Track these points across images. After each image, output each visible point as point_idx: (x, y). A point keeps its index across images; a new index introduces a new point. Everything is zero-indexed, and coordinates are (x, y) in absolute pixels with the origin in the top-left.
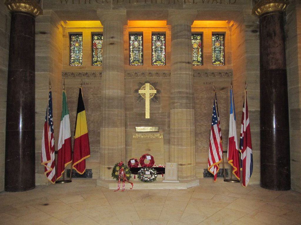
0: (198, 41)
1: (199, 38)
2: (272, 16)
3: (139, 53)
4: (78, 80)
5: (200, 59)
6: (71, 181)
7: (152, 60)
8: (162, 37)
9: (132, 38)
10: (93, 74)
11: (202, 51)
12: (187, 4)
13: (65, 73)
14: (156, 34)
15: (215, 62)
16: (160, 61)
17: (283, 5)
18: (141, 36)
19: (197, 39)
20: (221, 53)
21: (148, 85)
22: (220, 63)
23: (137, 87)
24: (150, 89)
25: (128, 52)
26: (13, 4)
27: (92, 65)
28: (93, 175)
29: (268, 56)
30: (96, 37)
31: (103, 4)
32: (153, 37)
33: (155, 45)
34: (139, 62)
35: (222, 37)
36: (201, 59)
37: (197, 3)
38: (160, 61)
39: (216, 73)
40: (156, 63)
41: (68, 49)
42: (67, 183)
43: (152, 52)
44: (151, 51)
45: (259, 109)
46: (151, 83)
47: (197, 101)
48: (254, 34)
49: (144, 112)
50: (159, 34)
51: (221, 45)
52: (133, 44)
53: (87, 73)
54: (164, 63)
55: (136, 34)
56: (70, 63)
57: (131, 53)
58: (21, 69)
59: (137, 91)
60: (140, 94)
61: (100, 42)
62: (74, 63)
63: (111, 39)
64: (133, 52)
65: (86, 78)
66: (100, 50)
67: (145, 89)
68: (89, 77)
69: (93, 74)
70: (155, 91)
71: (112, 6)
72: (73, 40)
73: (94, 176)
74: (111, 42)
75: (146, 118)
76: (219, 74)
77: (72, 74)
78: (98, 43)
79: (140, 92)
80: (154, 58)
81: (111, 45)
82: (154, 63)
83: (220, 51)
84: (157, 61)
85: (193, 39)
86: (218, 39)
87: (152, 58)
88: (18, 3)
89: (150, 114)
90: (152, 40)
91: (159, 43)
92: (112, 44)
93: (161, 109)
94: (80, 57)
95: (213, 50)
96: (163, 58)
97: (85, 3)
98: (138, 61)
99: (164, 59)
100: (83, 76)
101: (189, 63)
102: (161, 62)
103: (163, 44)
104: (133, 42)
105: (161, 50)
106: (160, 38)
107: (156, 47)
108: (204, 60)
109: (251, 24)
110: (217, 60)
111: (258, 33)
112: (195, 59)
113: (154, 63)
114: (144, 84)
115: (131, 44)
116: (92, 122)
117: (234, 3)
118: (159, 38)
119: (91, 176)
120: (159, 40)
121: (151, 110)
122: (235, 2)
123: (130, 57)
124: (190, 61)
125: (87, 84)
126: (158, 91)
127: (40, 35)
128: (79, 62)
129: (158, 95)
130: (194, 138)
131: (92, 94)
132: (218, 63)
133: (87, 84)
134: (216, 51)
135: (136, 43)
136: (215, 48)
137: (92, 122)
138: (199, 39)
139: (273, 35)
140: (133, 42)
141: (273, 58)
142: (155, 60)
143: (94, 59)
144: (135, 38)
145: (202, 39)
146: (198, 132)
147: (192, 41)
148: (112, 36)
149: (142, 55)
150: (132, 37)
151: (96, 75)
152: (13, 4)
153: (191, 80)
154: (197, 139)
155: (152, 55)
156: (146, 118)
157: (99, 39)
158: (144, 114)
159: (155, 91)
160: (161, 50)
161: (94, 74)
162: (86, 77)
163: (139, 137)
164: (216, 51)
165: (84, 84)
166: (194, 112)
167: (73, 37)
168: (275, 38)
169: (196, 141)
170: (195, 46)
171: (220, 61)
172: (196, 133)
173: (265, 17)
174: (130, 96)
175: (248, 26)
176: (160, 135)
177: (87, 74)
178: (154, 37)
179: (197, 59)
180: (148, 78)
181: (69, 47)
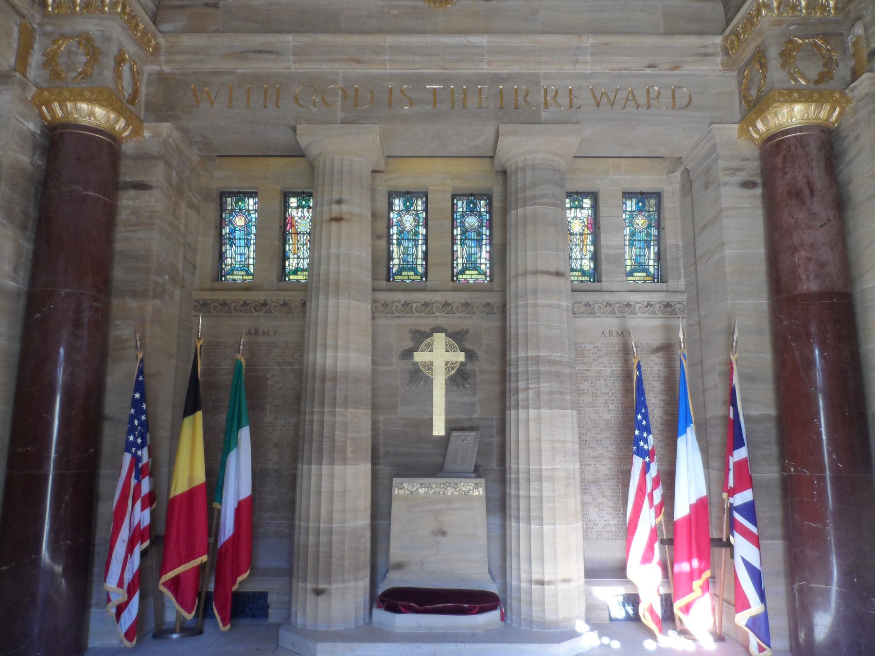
0: (586, 213)
1: (587, 203)
2: (800, 141)
3: (417, 247)
4: (244, 322)
5: (588, 265)
6: (200, 632)
7: (453, 268)
8: (482, 202)
9: (398, 204)
10: (282, 305)
11: (596, 242)
12: (551, 108)
13: (201, 302)
14: (464, 195)
15: (631, 274)
16: (413, 271)
17: (833, 110)
18: (422, 198)
19: (582, 208)
20: (649, 248)
21: (439, 339)
22: (648, 276)
23: (410, 344)
24: (447, 351)
25: (383, 243)
26: (56, 105)
27: (389, 280)
28: (270, 611)
29: (793, 254)
30: (293, 202)
31: (315, 109)
32: (455, 202)
33: (462, 224)
34: (416, 274)
35: (652, 201)
36: (592, 265)
37: (580, 107)
38: (411, 269)
39: (637, 303)
40: (465, 277)
41: (213, 232)
42: (189, 638)
43: (453, 243)
44: (450, 243)
45: (772, 412)
46: (450, 331)
47: (585, 385)
48: (747, 192)
49: (428, 416)
50: (471, 195)
51: (649, 226)
52: (400, 223)
53: (265, 301)
54: (486, 277)
55: (408, 193)
56: (453, 276)
57: (395, 248)
58: (66, 287)
59: (408, 354)
60: (416, 363)
61: (306, 214)
62: (233, 274)
63: (335, 207)
64: (399, 244)
65: (264, 316)
66: (305, 237)
67: (432, 351)
68: (271, 312)
69: (282, 305)
70: (461, 357)
71: (340, 115)
72: (229, 208)
73: (274, 614)
74: (334, 215)
75: (435, 433)
76: (646, 307)
77: (221, 305)
78: (300, 218)
79: (419, 357)
80: (460, 261)
81: (333, 223)
82: (458, 274)
83: (646, 241)
84: (469, 269)
85: (570, 208)
86: (644, 206)
87: (453, 260)
88: (70, 100)
89: (448, 421)
90: (453, 212)
91: (472, 221)
92: (338, 219)
93: (478, 409)
94: (249, 258)
95: (627, 238)
96: (483, 261)
97: (265, 107)
98: (414, 269)
99: (486, 264)
100: (253, 311)
101: (558, 274)
102: (479, 274)
103: (485, 221)
104: (400, 215)
105: (477, 240)
106: (475, 205)
107: (464, 232)
108: (604, 266)
109: (736, 164)
110: (640, 267)
111: (759, 191)
112: (575, 265)
113: (396, 277)
114: (430, 335)
115: (395, 220)
116: (276, 445)
117: (686, 107)
118: (471, 205)
119: (264, 614)
120: (472, 212)
121: (449, 411)
122: (690, 102)
123: (390, 258)
124: (561, 269)
125: (267, 334)
126: (471, 355)
127: (132, 193)
128: (247, 271)
129: (469, 367)
130: (579, 498)
131: (279, 364)
132: (639, 275)
133: (267, 334)
134: (635, 240)
135: (408, 221)
136: (633, 234)
137: (276, 445)
138: (589, 208)
139: (807, 193)
140: (400, 215)
141: (809, 259)
142: (460, 267)
143: (289, 265)
144: (404, 204)
145: (595, 207)
146: (590, 477)
147: (568, 211)
148: (336, 197)
149: (426, 254)
150: (396, 201)
151: (291, 307)
152: (56, 105)
153: (566, 325)
154: (587, 498)
155: (453, 252)
156: (435, 433)
157: (303, 207)
158: (429, 424)
159: (461, 357)
160: (477, 240)
161: (285, 304)
162: (262, 314)
163: (412, 493)
164: (635, 240)
165: (256, 333)
166: (575, 420)
167: (229, 200)
168: (812, 202)
169: (584, 504)
170: (576, 227)
171: (646, 271)
172: (582, 481)
173: (779, 143)
174: (389, 368)
175: (728, 169)
176: (477, 486)
177: (265, 304)
178: (460, 203)
179: (581, 265)
180: (441, 320)
181: (218, 230)
